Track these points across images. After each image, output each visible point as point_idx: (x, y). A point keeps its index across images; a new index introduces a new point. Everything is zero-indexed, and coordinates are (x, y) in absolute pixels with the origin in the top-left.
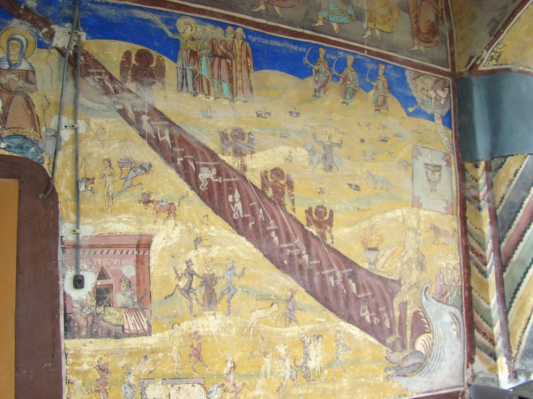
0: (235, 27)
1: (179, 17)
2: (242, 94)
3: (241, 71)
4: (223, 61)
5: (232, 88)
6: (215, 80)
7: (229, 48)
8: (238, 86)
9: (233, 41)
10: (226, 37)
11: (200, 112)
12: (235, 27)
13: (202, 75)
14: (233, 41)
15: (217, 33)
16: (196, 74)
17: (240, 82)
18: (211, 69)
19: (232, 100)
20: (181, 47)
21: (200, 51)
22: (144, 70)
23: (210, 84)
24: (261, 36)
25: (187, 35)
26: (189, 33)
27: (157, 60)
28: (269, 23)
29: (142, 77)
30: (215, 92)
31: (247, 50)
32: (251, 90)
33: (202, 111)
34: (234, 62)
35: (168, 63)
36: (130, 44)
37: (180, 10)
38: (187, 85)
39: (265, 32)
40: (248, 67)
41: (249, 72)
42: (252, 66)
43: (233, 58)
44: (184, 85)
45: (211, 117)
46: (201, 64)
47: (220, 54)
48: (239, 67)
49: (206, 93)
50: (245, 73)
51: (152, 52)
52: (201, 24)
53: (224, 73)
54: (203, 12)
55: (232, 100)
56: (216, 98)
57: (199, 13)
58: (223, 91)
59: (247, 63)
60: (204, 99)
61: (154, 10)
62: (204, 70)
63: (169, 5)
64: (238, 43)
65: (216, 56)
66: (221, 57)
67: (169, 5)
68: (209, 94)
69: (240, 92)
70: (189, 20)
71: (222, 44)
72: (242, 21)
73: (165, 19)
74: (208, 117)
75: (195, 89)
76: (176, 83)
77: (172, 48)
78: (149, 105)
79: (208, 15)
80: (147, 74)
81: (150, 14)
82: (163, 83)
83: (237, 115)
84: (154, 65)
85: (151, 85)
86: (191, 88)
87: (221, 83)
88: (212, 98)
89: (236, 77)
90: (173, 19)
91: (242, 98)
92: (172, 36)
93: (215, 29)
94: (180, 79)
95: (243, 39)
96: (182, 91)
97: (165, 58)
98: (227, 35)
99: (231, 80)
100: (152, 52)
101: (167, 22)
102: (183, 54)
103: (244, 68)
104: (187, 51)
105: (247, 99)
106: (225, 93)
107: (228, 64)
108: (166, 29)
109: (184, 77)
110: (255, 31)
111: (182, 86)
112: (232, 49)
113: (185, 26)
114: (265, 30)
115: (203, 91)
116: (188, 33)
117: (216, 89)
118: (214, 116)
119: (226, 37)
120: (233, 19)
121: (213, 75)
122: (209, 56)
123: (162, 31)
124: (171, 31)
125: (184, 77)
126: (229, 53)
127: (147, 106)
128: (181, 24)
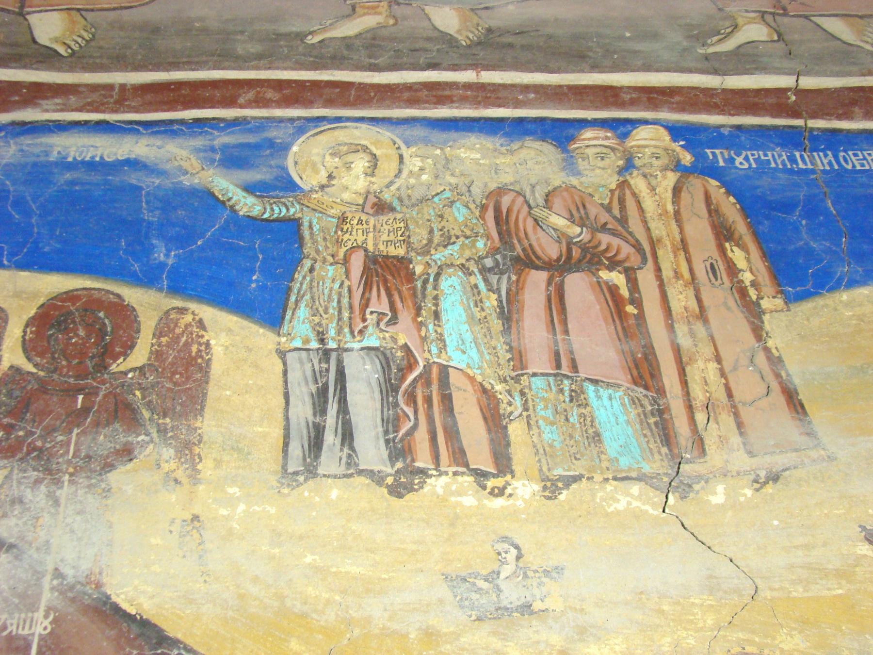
0: (621, 128)
1: (301, 131)
2: (736, 440)
3: (702, 315)
4: (578, 287)
5: (662, 412)
6: (538, 383)
7: (604, 217)
8: (698, 395)
9: (623, 185)
10: (578, 174)
11: (443, 591)
12: (621, 128)
13: (444, 370)
14: (623, 185)
15: (532, 165)
16: (411, 365)
17: (703, 371)
18: (507, 330)
19: (676, 484)
20: (308, 248)
21: (425, 251)
22: (71, 392)
23: (504, 408)
24: (783, 146)
25: (346, 196)
26: (361, 184)
27: (158, 334)
28: (808, 82)
29: (50, 431)
30: (542, 451)
31: (713, 211)
32: (793, 400)
33: (455, 580)
34: (646, 278)
35: (227, 336)
36: (323, 452)
37: (308, 103)
38: (347, 436)
39: (799, 122)
40: (743, 293)
41: (754, 312)
42: (764, 277)
43: (635, 260)
44: (330, 438)
45: (526, 609)
46: (437, 315)
47: (552, 251)
48: (681, 299)
49: (480, 456)
50: (729, 323)
51: (132, 295)
52: (426, 141)
53: (594, 341)
54: (438, 93)
55: (676, 484)
56: (552, 487)
57: (413, 102)
58: (597, 437)
59: (732, 270)
60: (469, 501)
61: (171, 122)
62: (459, 334)
63: (251, 95)
64: (654, 192)
65: (528, 261)
66: (560, 267)
67: (251, 95)
68: (503, 463)
69: (718, 431)
70: (362, 134)
71: (557, 203)
72: (653, 97)
73: (225, 147)
74: (501, 612)
75: (399, 450)
76: (277, 433)
77: (254, 268)
78: (66, 590)
79: (464, 100)
80: (86, 410)
81: (144, 141)
82: (188, 450)
83: (727, 569)
84: (139, 356)
85: (108, 467)
86: (371, 449)
87: (577, 397)
88: (524, 489)
89: (677, 351)
90: (271, 144)
91: (740, 460)
92: (256, 211)
93: (511, 152)
94: (302, 411)
95: (677, 166)
96: (311, 472)
97: (207, 312)
98: (582, 165)
99: (644, 372)
100: (132, 295)
101: (233, 160)
102: (324, 282)
103: (717, 296)
104: (346, 261)
105: (780, 461)
106: (611, 446)
107: (613, 290)
108: (225, 184)
109: (331, 391)
110: (739, 128)
111: (316, 443)
112: (623, 221)
113: (333, 162)
114: (796, 115)
115: (460, 457)
116: (355, 181)
117: (550, 434)
118: (554, 603)
119: (578, 174)
120: (609, 95)
121: (519, 359)
122: (484, 271)
123: (209, 199)
124: (249, 189)
125: (331, 391)
126: (605, 239)
127: (47, 597)
128: (311, 158)
